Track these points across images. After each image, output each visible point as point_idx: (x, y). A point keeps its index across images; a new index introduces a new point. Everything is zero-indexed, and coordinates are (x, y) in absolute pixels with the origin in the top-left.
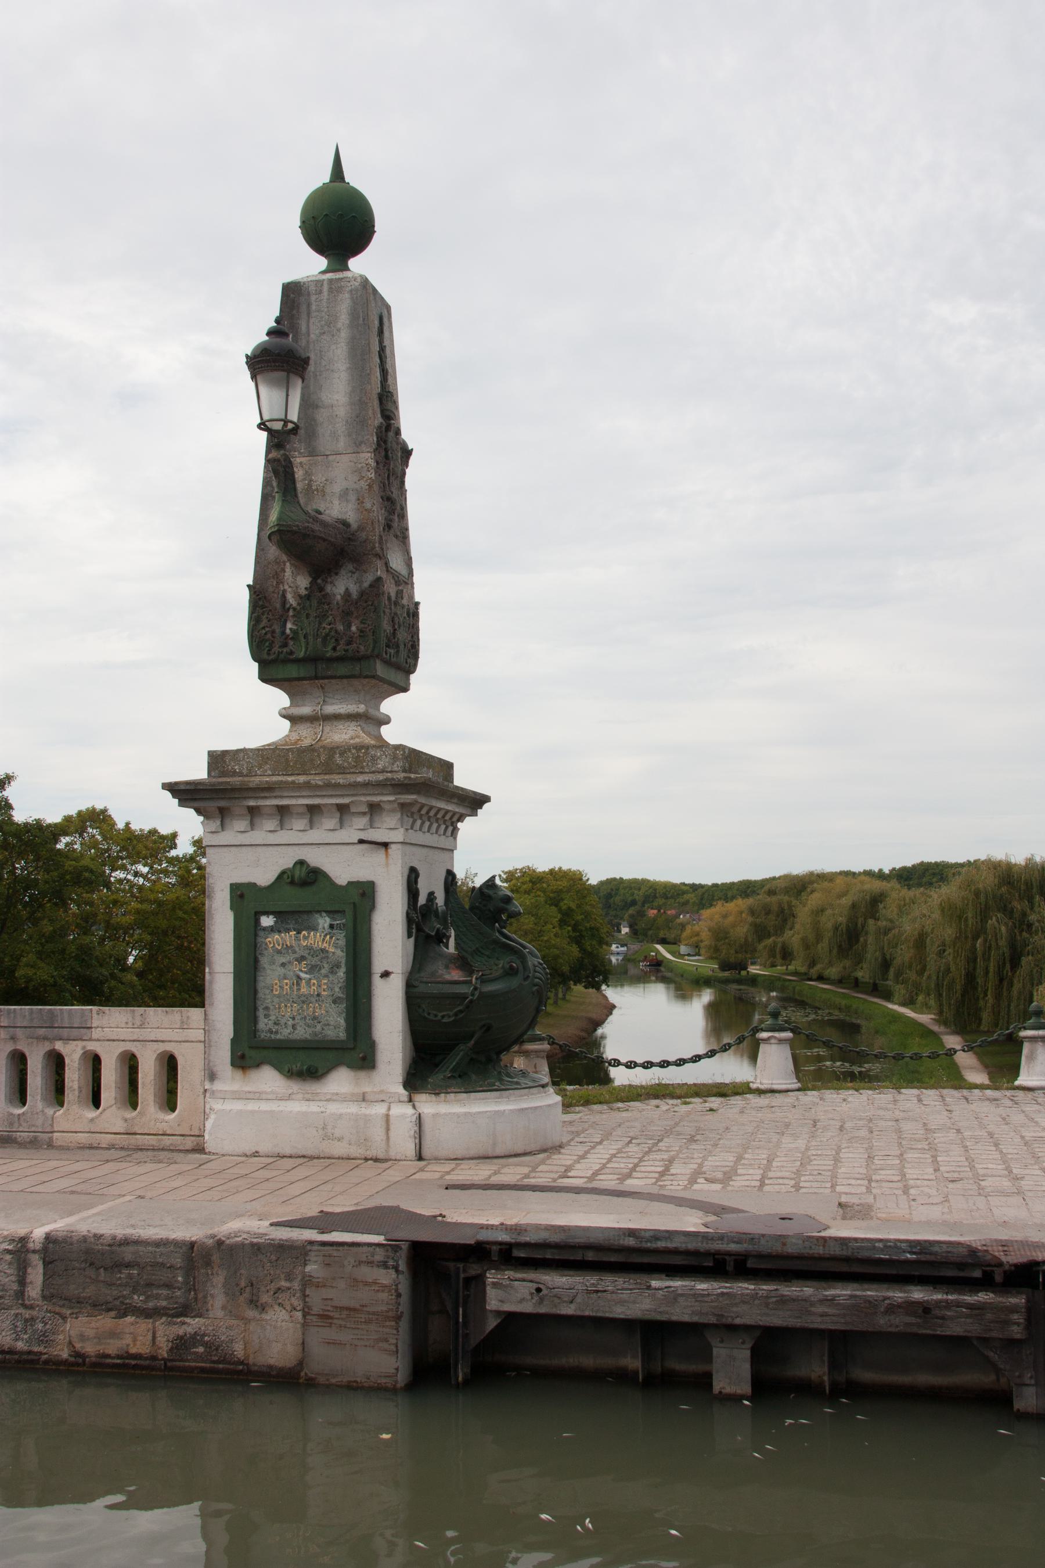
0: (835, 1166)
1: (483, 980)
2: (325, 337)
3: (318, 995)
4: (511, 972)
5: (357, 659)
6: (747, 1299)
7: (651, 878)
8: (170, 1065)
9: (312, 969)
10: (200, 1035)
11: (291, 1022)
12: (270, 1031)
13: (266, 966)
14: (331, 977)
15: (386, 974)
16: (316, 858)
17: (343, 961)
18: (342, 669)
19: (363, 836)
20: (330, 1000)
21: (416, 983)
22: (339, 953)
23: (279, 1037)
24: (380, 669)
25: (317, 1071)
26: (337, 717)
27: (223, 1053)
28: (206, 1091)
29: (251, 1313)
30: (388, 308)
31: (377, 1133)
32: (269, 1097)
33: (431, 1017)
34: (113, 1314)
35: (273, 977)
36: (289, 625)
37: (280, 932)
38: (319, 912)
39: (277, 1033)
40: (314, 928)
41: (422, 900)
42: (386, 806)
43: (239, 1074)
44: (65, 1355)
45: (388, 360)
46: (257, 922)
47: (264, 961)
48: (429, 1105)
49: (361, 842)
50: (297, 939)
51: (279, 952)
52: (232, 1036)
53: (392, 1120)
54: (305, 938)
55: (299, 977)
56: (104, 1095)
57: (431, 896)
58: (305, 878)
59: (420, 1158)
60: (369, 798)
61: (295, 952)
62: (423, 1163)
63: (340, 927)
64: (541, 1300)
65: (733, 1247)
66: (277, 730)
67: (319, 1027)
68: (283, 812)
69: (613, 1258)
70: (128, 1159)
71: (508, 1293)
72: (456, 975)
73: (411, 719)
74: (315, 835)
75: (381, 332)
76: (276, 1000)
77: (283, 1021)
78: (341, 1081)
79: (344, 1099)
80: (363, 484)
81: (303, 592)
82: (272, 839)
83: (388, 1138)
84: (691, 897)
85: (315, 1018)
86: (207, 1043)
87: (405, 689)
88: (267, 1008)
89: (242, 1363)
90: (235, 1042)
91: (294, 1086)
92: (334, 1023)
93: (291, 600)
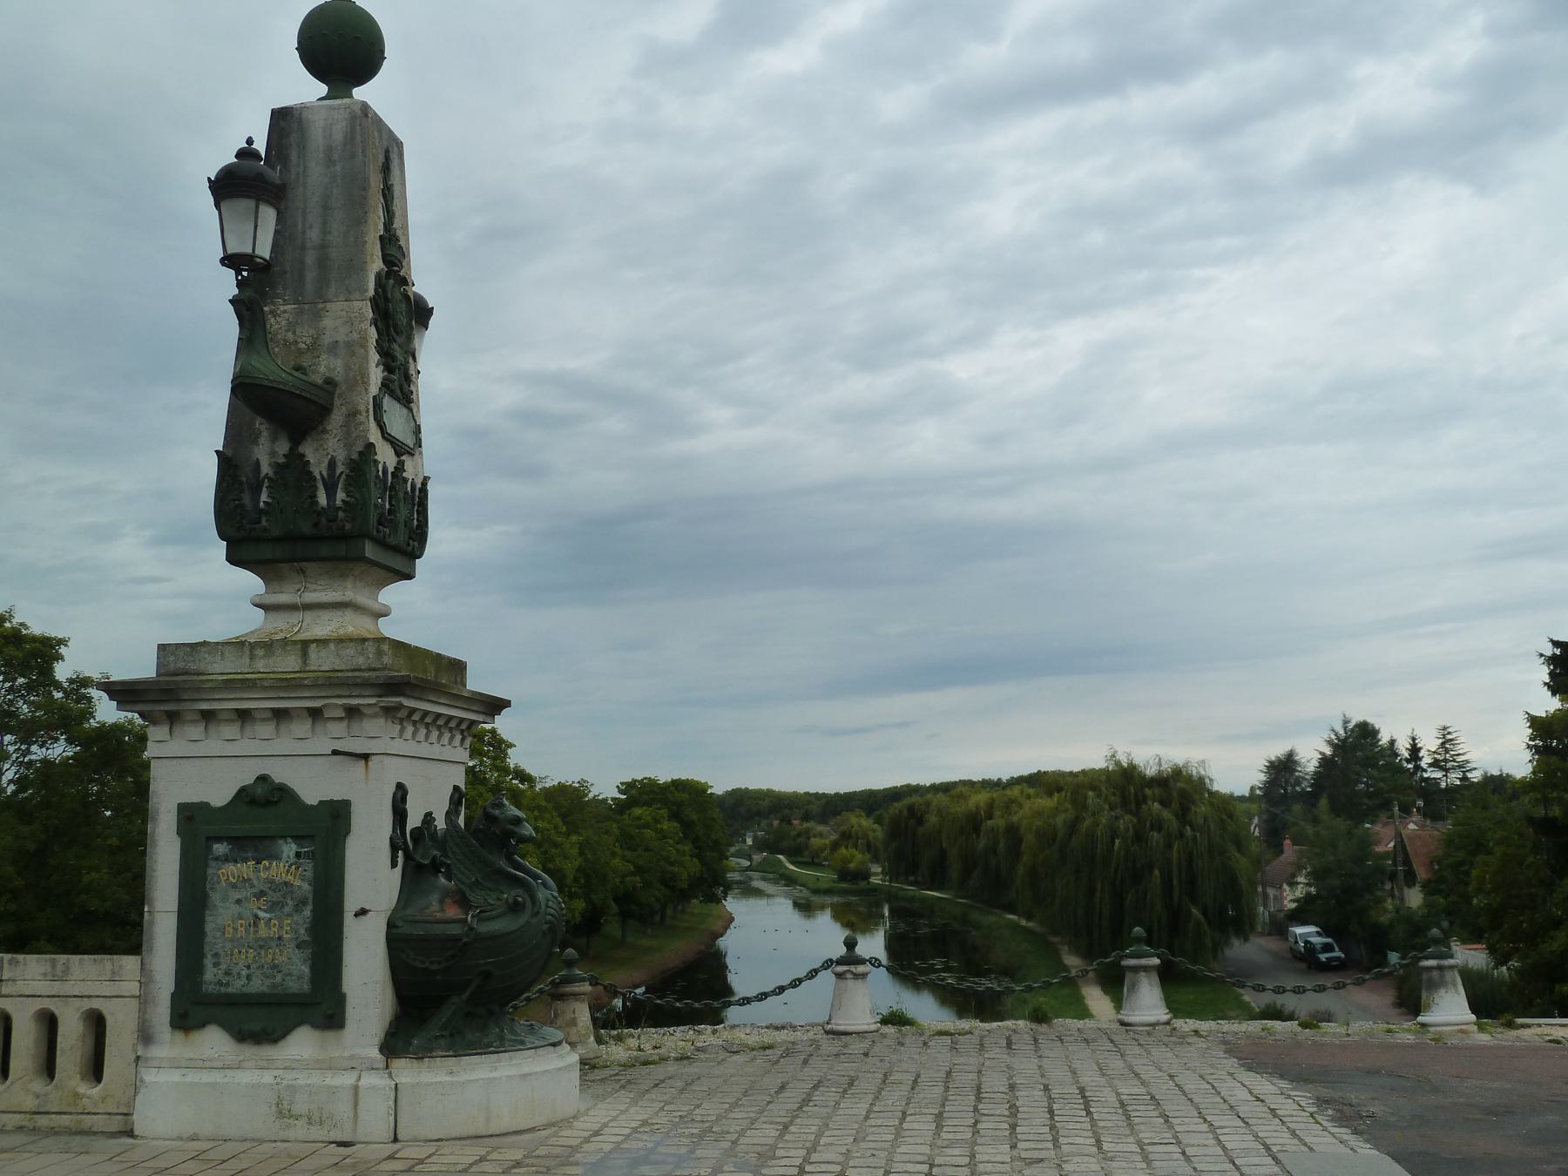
0: (895, 1143)
1: (480, 918)
3: (280, 938)
4: (515, 908)
5: (344, 537)
7: (776, 789)
8: (97, 1023)
9: (274, 906)
10: (134, 988)
12: (220, 983)
15: (362, 912)
16: (281, 773)
17: (311, 896)
18: (325, 550)
19: (339, 746)
20: (293, 944)
21: (400, 923)
22: (306, 886)
23: (230, 990)
24: (370, 550)
27: (162, 1011)
28: (138, 1058)
30: (400, 145)
31: (343, 1108)
32: (215, 1064)
35: (223, 917)
36: (264, 497)
37: (236, 862)
38: (284, 837)
39: (227, 985)
40: (278, 858)
41: (414, 821)
42: (366, 711)
43: (180, 1035)
45: (396, 201)
46: (209, 849)
47: (215, 897)
48: (407, 1072)
49: (335, 753)
50: (256, 870)
51: (234, 886)
53: (361, 1094)
54: (266, 869)
55: (256, 916)
56: (60, 1061)
57: (428, 818)
59: (396, 1140)
60: (345, 701)
61: (253, 886)
62: (397, 1146)
66: (246, 621)
67: (279, 978)
68: (315, 714)
70: (29, 1147)
72: (453, 912)
73: (413, 611)
74: (284, 744)
75: (386, 169)
76: (228, 945)
77: (235, 972)
78: (302, 1043)
79: (307, 1066)
81: (282, 460)
82: (230, 749)
83: (356, 1115)
84: (814, 808)
85: (274, 967)
86: (144, 1000)
87: (410, 577)
88: (216, 955)
90: (175, 997)
91: (249, 1051)
92: (296, 971)
93: (266, 469)
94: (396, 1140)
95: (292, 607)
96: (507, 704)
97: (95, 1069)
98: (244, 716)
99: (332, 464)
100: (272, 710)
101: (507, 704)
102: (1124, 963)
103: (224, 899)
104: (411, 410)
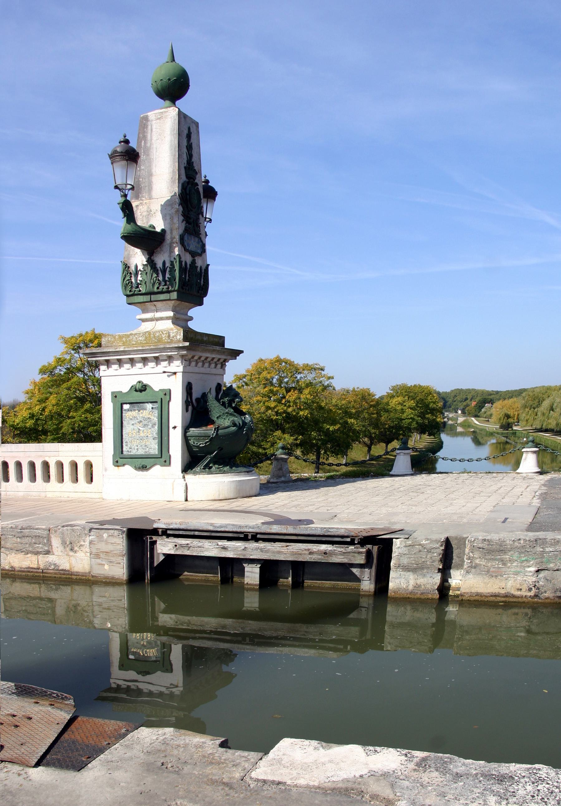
2: (158, 141)
6: (255, 550)
8: (89, 466)
11: (136, 448)
13: (126, 425)
14: (152, 429)
15: (175, 427)
20: (152, 438)
23: (131, 453)
25: (146, 467)
26: (161, 319)
29: (71, 553)
30: (197, 124)
33: (195, 444)
34: (23, 553)
35: (128, 429)
40: (146, 409)
44: (7, 568)
48: (190, 477)
51: (131, 419)
52: (113, 453)
54: (142, 413)
58: (143, 388)
59: (186, 500)
61: (137, 419)
63: (155, 408)
64: (177, 549)
65: (251, 530)
67: (147, 449)
69: (205, 534)
71: (165, 547)
76: (130, 439)
80: (173, 211)
85: (146, 446)
88: (126, 442)
89: (69, 571)
92: (153, 448)
94: (186, 500)
95: (151, 320)
96: (242, 352)
97: (90, 479)
98: (132, 361)
99: (164, 263)
100: (142, 358)
101: (242, 352)
102: (523, 450)
103: (128, 424)
104: (201, 239)
